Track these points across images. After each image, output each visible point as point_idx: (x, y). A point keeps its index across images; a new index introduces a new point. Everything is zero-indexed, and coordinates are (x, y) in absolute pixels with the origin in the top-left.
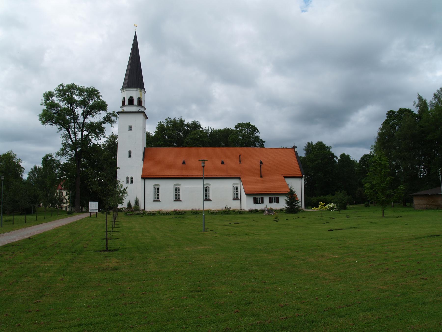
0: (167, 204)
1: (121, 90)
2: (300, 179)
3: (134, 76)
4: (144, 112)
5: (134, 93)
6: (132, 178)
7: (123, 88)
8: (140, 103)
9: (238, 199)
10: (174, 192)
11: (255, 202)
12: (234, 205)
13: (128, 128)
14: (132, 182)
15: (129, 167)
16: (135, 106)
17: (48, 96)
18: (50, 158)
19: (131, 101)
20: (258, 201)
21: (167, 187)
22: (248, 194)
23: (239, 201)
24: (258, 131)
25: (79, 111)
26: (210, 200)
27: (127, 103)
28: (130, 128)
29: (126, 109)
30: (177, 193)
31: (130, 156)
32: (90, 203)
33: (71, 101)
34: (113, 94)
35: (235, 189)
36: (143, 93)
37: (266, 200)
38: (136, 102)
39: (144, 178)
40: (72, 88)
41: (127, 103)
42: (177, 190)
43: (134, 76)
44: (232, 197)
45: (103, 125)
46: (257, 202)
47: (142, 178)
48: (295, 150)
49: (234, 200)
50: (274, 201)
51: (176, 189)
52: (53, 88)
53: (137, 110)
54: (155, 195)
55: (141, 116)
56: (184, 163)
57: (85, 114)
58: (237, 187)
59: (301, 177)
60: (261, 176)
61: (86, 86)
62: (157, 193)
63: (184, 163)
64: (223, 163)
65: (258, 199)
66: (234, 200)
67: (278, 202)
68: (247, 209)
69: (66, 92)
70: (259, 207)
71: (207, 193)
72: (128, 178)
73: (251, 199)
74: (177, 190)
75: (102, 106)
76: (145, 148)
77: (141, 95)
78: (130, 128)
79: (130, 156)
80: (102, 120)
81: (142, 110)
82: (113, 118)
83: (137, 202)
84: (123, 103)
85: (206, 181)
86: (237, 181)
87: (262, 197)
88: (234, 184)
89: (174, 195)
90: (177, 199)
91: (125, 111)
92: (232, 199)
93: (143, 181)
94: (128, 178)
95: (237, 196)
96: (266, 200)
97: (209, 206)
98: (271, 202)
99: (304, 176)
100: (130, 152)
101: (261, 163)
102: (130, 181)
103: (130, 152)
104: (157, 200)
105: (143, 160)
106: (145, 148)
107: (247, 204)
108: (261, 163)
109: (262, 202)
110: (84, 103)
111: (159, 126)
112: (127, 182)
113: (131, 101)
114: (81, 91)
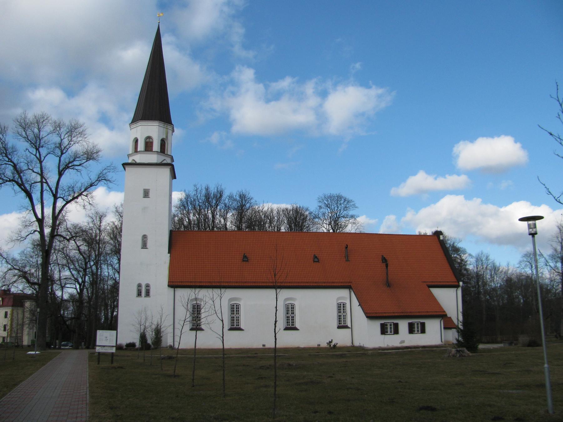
2: (455, 289)
4: (173, 166)
5: (152, 129)
6: (148, 286)
7: (135, 120)
9: (346, 327)
10: (230, 313)
11: (384, 331)
12: (342, 338)
13: (142, 193)
14: (148, 294)
15: (144, 266)
20: (416, 329)
22: (371, 316)
23: (349, 331)
24: (355, 206)
26: (240, 329)
27: (141, 146)
28: (146, 194)
29: (138, 158)
31: (144, 246)
32: (98, 331)
35: (341, 307)
37: (403, 325)
38: (156, 146)
39: (173, 285)
42: (235, 309)
44: (335, 323)
46: (387, 332)
47: (169, 286)
48: (439, 238)
51: (194, 307)
53: (159, 162)
55: (166, 171)
56: (245, 259)
58: (344, 305)
59: (457, 286)
64: (316, 259)
65: (416, 326)
66: (339, 327)
67: (423, 331)
72: (139, 286)
73: (376, 325)
78: (146, 194)
79: (144, 246)
81: (168, 161)
82: (110, 176)
83: (158, 332)
85: (285, 294)
86: (343, 294)
88: (338, 299)
89: (230, 318)
92: (189, 329)
93: (172, 289)
94: (139, 286)
96: (403, 325)
98: (411, 331)
100: (145, 237)
101: (384, 260)
102: (144, 291)
103: (145, 237)
105: (170, 251)
108: (384, 260)
109: (396, 332)
112: (139, 294)
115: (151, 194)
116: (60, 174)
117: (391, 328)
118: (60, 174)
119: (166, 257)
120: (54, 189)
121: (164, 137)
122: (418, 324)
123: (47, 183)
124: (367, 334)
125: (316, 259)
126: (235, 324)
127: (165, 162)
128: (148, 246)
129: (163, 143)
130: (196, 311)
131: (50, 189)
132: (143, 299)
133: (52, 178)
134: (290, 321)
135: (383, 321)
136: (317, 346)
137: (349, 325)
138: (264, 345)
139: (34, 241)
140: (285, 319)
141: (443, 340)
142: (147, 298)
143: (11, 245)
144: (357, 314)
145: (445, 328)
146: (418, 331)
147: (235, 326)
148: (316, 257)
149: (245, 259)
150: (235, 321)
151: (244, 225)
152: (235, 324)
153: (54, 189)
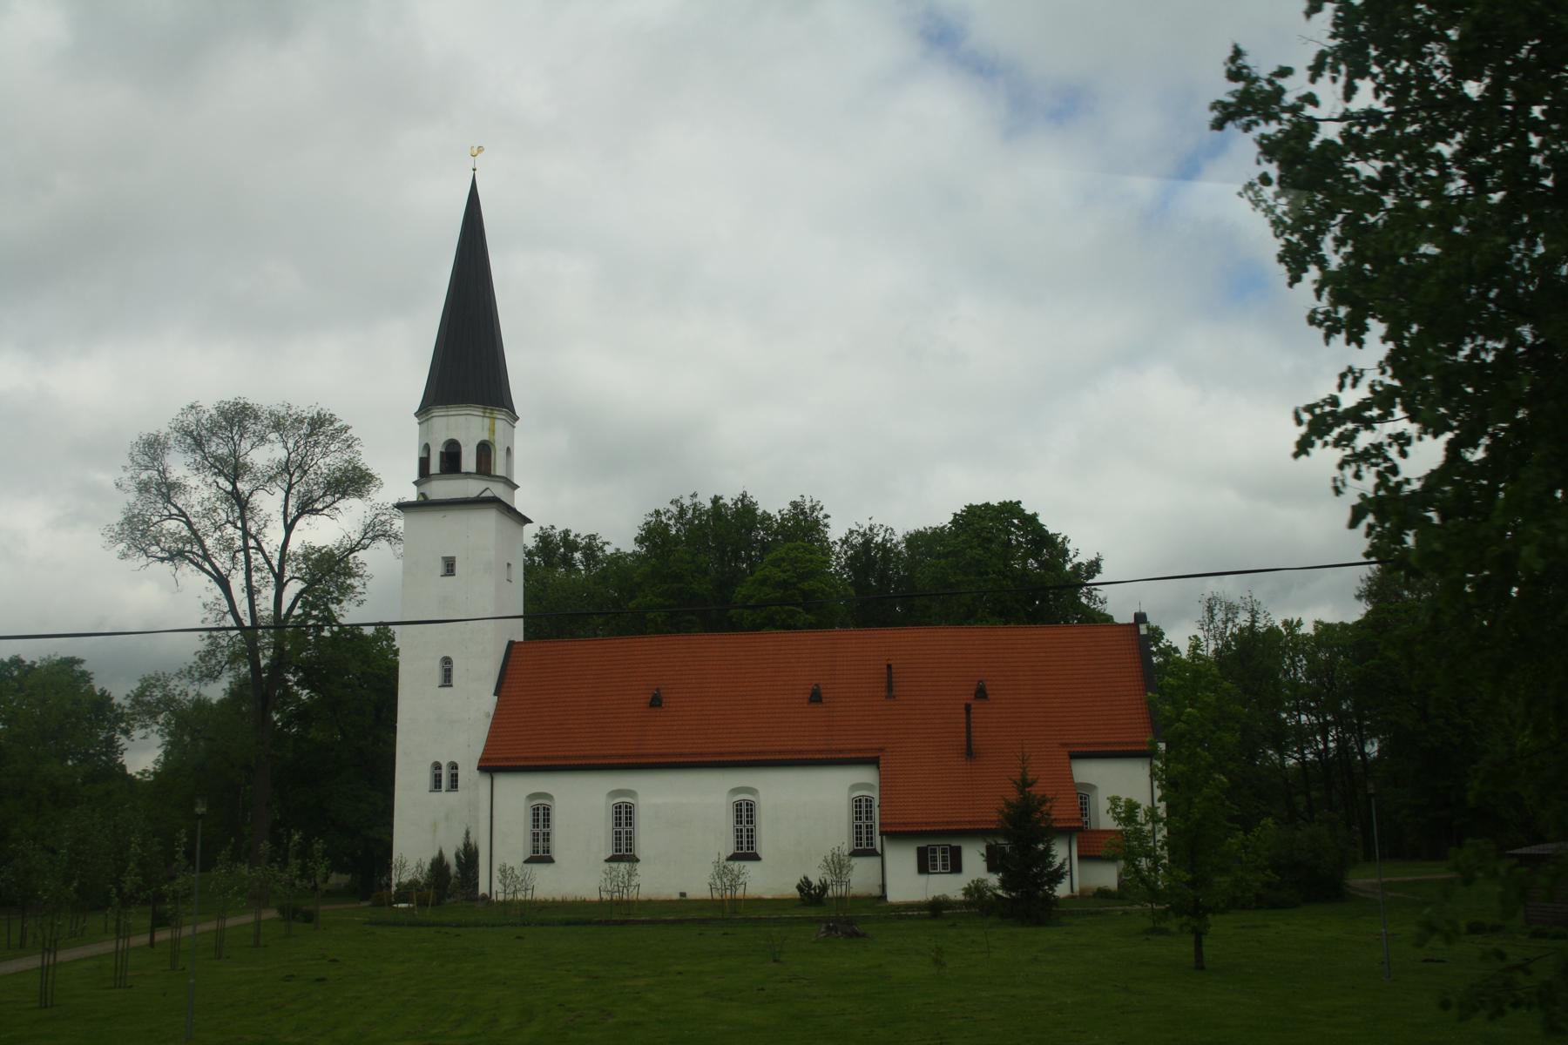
0: (576, 875)
1: (417, 414)
3: (469, 361)
5: (467, 427)
6: (454, 766)
7: (424, 411)
8: (484, 465)
10: (610, 824)
13: (440, 568)
14: (454, 785)
15: (441, 717)
16: (461, 477)
17: (153, 448)
18: (158, 693)
19: (451, 460)
20: (939, 863)
21: (582, 802)
27: (435, 466)
28: (449, 567)
29: (443, 489)
30: (541, 830)
31: (447, 680)
36: (500, 425)
40: (237, 417)
41: (435, 466)
42: (624, 816)
43: (469, 361)
45: (361, 555)
46: (935, 867)
50: (939, 863)
51: (618, 809)
52: (161, 424)
54: (535, 837)
56: (656, 702)
59: (1146, 754)
60: (970, 752)
62: (624, 829)
63: (656, 702)
64: (816, 697)
65: (939, 855)
69: (222, 434)
71: (744, 827)
72: (437, 766)
74: (624, 816)
76: (511, 644)
77: (492, 431)
78: (449, 567)
79: (447, 680)
80: (356, 537)
84: (424, 464)
87: (955, 844)
88: (854, 787)
90: (624, 853)
93: (484, 781)
94: (437, 766)
95: (870, 839)
97: (759, 881)
99: (1162, 746)
100: (447, 661)
103: (447, 661)
104: (541, 856)
106: (511, 644)
109: (956, 868)
112: (437, 784)
113: (451, 460)
116: (289, 528)
117: (944, 859)
118: (289, 528)
119: (489, 702)
120: (275, 563)
121: (485, 436)
122: (944, 851)
123: (260, 548)
126: (623, 848)
127: (487, 494)
129: (484, 450)
130: (541, 816)
131: (269, 563)
132: (444, 796)
133: (273, 538)
134: (745, 840)
135: (923, 844)
136: (676, 896)
137: (879, 849)
138: (683, 894)
140: (529, 838)
141: (1076, 888)
142: (452, 796)
145: (1081, 858)
146: (189, 854)
147: (623, 852)
150: (623, 842)
152: (623, 848)
153: (275, 563)
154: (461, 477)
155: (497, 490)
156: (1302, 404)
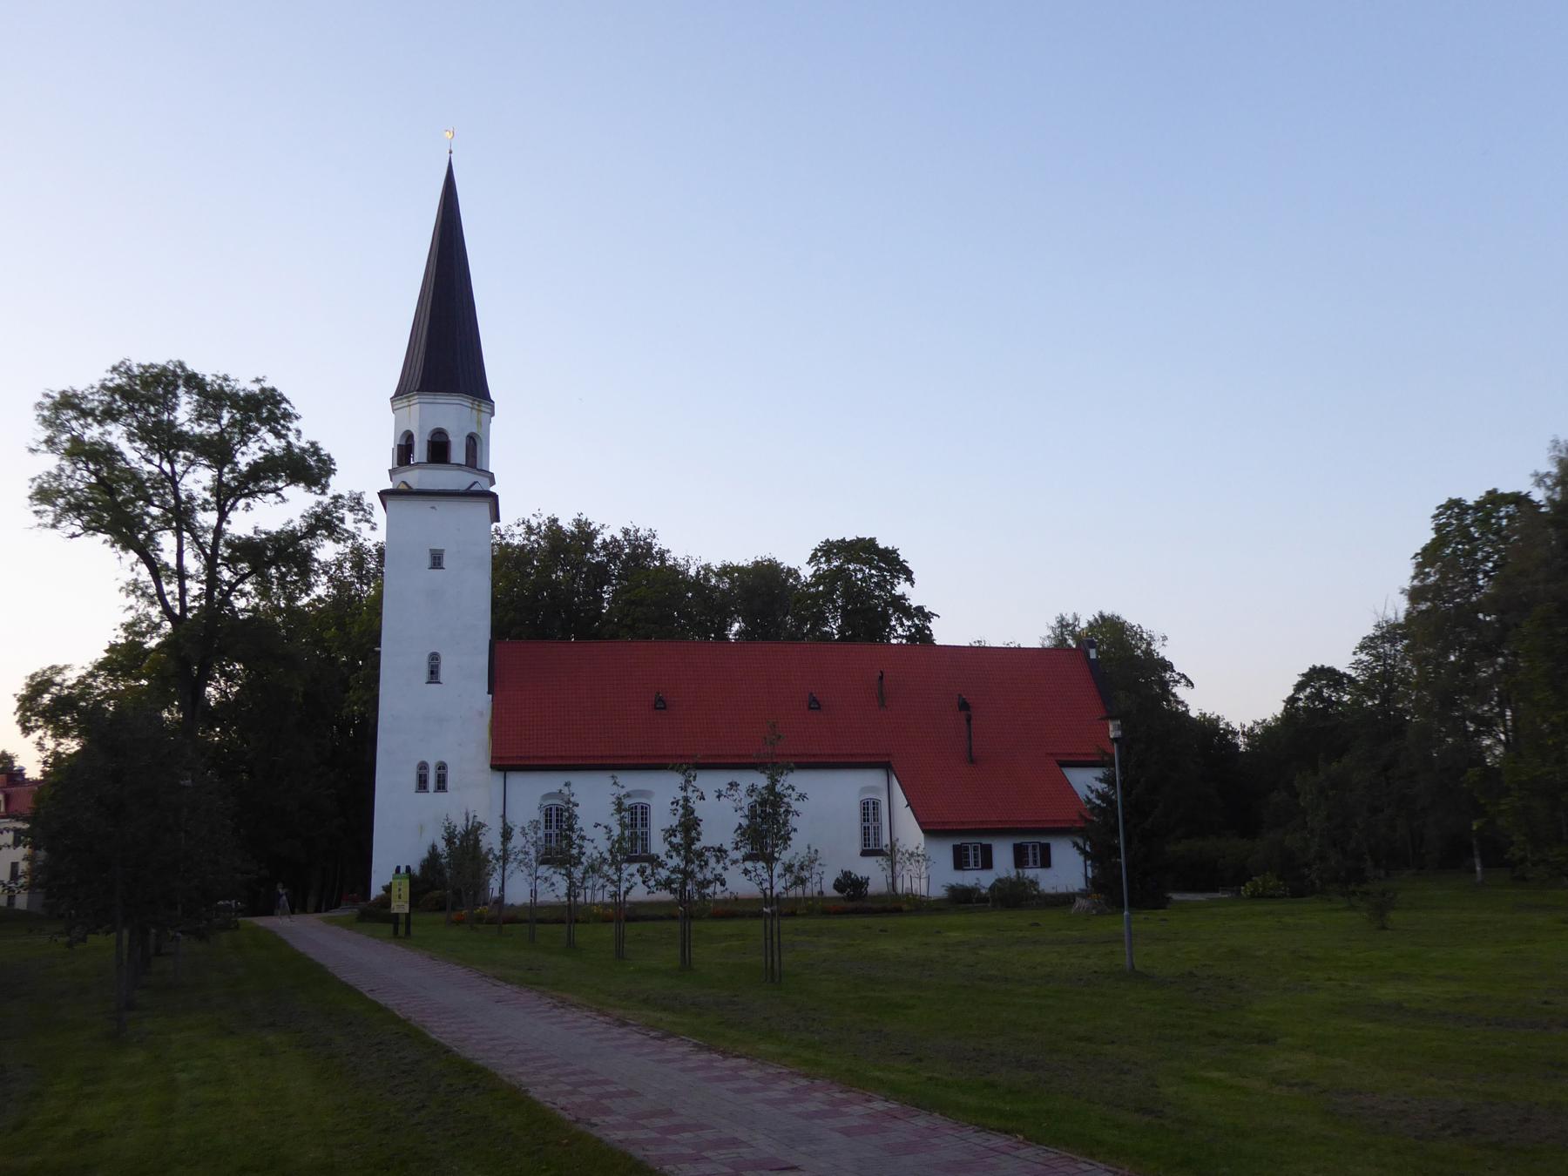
1: (393, 400)
3: (446, 352)
5: (449, 413)
6: (442, 767)
7: (402, 392)
11: (960, 862)
13: (428, 562)
14: (441, 785)
16: (441, 464)
19: (439, 450)
20: (1031, 858)
24: (909, 578)
25: (198, 480)
27: (420, 452)
28: (437, 561)
29: (415, 478)
31: (434, 675)
33: (165, 439)
34: (354, 420)
35: (869, 810)
37: (1003, 854)
39: (503, 764)
43: (446, 352)
44: (857, 847)
49: (864, 853)
50: (1031, 858)
56: (660, 704)
57: (225, 497)
58: (876, 804)
61: (244, 383)
65: (971, 853)
66: (864, 853)
68: (938, 892)
69: (145, 393)
70: (981, 879)
72: (423, 766)
73: (943, 852)
75: (307, 468)
78: (437, 561)
79: (434, 675)
86: (870, 782)
91: (415, 486)
93: (499, 776)
94: (423, 766)
95: (877, 840)
96: (1003, 854)
100: (434, 658)
102: (432, 779)
103: (434, 658)
107: (927, 869)
108: (964, 706)
109: (987, 864)
110: (217, 451)
111: (679, 573)
112: (422, 784)
113: (439, 450)
114: (213, 398)
115: (446, 562)
122: (975, 849)
124: (927, 869)
125: (815, 704)
126: (639, 849)
128: (445, 564)
132: (431, 796)
135: (958, 842)
139: (1102, 616)
142: (441, 795)
143: (400, 477)
144: (909, 833)
148: (814, 700)
149: (660, 704)
151: (736, 627)
154: (441, 464)
155: (483, 484)
156: (88, 375)
